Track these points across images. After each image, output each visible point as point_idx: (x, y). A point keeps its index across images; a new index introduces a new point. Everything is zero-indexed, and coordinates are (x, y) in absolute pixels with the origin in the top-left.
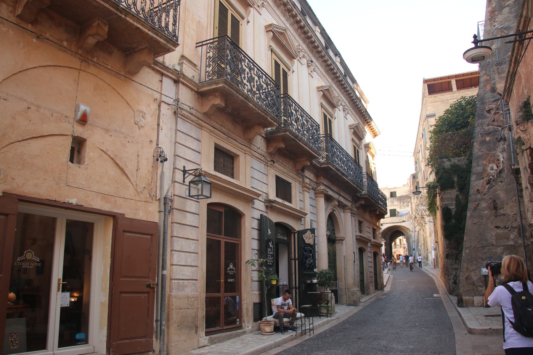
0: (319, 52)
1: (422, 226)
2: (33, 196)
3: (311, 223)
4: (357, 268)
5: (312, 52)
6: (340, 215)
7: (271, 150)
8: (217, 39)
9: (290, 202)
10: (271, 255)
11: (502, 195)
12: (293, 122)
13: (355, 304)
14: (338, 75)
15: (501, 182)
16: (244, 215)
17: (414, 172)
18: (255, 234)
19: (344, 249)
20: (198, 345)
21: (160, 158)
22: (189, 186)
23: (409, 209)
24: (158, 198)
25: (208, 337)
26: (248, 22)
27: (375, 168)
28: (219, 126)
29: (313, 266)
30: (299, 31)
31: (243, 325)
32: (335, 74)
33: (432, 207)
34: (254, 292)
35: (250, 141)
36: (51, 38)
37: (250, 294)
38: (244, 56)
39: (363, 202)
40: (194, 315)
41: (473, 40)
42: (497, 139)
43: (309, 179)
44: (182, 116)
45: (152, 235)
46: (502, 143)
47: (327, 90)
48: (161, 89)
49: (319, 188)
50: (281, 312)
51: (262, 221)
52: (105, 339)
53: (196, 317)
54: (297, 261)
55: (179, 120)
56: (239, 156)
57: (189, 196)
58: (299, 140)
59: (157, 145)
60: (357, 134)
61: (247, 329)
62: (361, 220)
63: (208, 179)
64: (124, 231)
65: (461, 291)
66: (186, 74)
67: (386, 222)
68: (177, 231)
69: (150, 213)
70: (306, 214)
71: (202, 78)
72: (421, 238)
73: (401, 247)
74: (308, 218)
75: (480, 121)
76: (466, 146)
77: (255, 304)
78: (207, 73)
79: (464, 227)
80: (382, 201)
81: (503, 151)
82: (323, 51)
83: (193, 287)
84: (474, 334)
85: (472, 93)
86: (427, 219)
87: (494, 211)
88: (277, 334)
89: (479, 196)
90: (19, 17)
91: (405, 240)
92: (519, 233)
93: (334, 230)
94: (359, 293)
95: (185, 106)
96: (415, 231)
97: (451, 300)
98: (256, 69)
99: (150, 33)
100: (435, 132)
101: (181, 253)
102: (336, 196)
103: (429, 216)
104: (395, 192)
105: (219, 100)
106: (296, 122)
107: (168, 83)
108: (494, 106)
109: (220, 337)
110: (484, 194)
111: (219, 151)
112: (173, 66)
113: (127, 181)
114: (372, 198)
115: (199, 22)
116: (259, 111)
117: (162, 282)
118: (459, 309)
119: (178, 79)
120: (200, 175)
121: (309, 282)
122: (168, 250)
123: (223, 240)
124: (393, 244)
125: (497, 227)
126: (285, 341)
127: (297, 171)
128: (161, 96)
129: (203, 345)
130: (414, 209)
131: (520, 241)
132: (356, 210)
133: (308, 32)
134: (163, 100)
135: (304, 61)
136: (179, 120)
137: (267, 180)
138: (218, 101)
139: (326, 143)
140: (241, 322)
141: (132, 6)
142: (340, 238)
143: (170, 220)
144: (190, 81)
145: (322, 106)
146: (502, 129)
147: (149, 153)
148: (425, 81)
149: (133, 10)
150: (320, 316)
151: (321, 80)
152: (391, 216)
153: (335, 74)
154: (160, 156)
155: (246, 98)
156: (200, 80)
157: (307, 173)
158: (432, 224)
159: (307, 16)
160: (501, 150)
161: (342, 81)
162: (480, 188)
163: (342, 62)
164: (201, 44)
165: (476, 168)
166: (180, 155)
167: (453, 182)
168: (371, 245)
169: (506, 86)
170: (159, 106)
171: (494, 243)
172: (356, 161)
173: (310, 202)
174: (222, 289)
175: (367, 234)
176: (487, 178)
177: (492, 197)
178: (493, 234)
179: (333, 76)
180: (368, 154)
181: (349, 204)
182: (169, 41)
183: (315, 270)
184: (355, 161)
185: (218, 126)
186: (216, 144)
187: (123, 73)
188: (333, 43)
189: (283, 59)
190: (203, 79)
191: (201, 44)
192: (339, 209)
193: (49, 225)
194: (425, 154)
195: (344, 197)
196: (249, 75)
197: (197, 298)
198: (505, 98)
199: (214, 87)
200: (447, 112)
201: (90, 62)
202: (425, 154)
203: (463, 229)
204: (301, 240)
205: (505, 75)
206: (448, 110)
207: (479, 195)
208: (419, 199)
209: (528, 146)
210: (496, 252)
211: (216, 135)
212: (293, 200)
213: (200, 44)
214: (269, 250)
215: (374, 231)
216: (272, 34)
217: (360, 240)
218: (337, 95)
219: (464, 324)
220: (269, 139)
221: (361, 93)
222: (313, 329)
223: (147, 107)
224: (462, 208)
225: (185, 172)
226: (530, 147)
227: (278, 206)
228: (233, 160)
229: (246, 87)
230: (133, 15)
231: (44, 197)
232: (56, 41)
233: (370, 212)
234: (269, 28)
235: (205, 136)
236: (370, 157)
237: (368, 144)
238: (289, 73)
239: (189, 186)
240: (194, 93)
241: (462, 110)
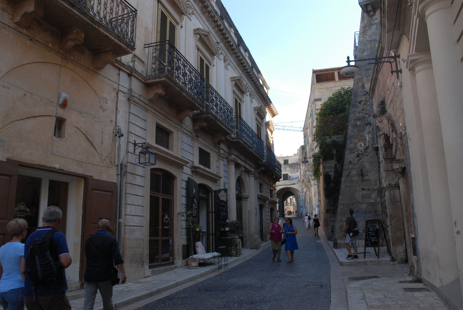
1: (308, 188)
2: (28, 162)
4: (258, 220)
5: (228, 49)
6: (246, 179)
7: (196, 128)
8: (159, 43)
9: (209, 167)
11: (367, 165)
12: (214, 107)
13: (256, 248)
15: (367, 156)
16: (176, 177)
17: (303, 144)
18: (184, 192)
21: (118, 134)
22: (139, 156)
23: (298, 174)
24: (116, 164)
25: (151, 270)
26: (182, 27)
27: (273, 141)
29: (226, 217)
30: (219, 33)
31: (175, 261)
33: (316, 173)
34: (183, 237)
35: (181, 121)
36: (40, 41)
37: (180, 239)
38: (193, 69)
39: (263, 169)
41: (347, 60)
42: (365, 123)
44: (134, 102)
45: (112, 192)
46: (368, 126)
47: (239, 80)
48: (119, 81)
49: (230, 157)
51: (189, 182)
52: (78, 270)
54: (214, 214)
55: (132, 104)
56: (173, 132)
57: (139, 163)
58: (218, 121)
59: (116, 124)
60: (260, 115)
61: (178, 265)
63: (154, 151)
64: (93, 189)
65: (336, 236)
66: (137, 69)
67: (280, 185)
68: (130, 189)
69: (110, 175)
70: (221, 178)
72: (308, 198)
73: (291, 205)
74: (222, 181)
75: (354, 109)
76: (342, 128)
77: (183, 246)
79: (340, 189)
80: (278, 168)
81: (369, 133)
82: (236, 49)
84: (344, 265)
85: (349, 84)
86: (312, 182)
87: (361, 177)
88: (201, 268)
89: (351, 166)
90: (17, 23)
91: (294, 199)
92: (378, 194)
94: (259, 240)
96: (303, 192)
97: (329, 245)
98: (182, 60)
99: (116, 40)
100: (320, 114)
101: (132, 206)
102: (243, 164)
103: (314, 180)
105: (161, 90)
106: (216, 107)
107: (123, 76)
108: (364, 99)
110: (355, 165)
111: (159, 128)
112: (128, 63)
113: (95, 151)
115: (146, 27)
117: (119, 227)
118: (335, 250)
119: (131, 73)
120: (147, 148)
121: (223, 230)
122: (123, 203)
123: (161, 196)
125: (363, 189)
126: (207, 273)
128: (119, 86)
130: (302, 174)
131: (379, 200)
132: (258, 175)
133: (226, 34)
134: (120, 89)
135: (222, 57)
136: (132, 104)
138: (160, 91)
139: (237, 122)
140: (173, 259)
141: (103, 19)
143: (124, 181)
145: (234, 93)
146: (369, 116)
147: (109, 130)
148: (314, 72)
149: (91, 13)
150: (231, 256)
151: (234, 72)
152: (284, 179)
154: (118, 132)
156: (147, 74)
157: (222, 146)
158: (316, 186)
159: (225, 20)
160: (367, 132)
161: (250, 72)
162: (351, 160)
164: (148, 46)
165: (349, 145)
166: (132, 132)
167: (333, 154)
169: (371, 87)
170: (117, 94)
171: (361, 201)
172: (259, 136)
174: (160, 234)
175: (266, 194)
176: (357, 153)
177: (360, 167)
178: (360, 194)
179: (243, 68)
180: (268, 130)
181: (253, 170)
182: (128, 45)
183: (227, 221)
184: (258, 136)
185: (158, 109)
186: (157, 123)
187: (92, 68)
188: (243, 42)
191: (148, 46)
192: (245, 174)
193: (37, 183)
194: (312, 130)
195: (249, 165)
196: (177, 65)
198: (370, 95)
199: (158, 80)
200: (330, 99)
201: (68, 59)
202: (312, 130)
203: (339, 190)
204: (217, 198)
205: (370, 78)
206: (331, 98)
207: (351, 165)
208: (307, 166)
209: (383, 133)
210: (362, 208)
212: (211, 166)
213: (147, 46)
214: (194, 205)
215: (271, 191)
216: (199, 36)
217: (261, 199)
218: (245, 83)
219: (338, 259)
220: (195, 120)
221: (264, 81)
222: (227, 265)
223: (109, 95)
224: (339, 174)
225: (135, 144)
226: (384, 133)
227: (200, 171)
228: (168, 135)
230: (104, 27)
231: (36, 163)
232: (43, 43)
234: (197, 32)
236: (269, 133)
237: (268, 122)
238: (210, 67)
239: (139, 156)
240: (142, 84)
241: (341, 98)
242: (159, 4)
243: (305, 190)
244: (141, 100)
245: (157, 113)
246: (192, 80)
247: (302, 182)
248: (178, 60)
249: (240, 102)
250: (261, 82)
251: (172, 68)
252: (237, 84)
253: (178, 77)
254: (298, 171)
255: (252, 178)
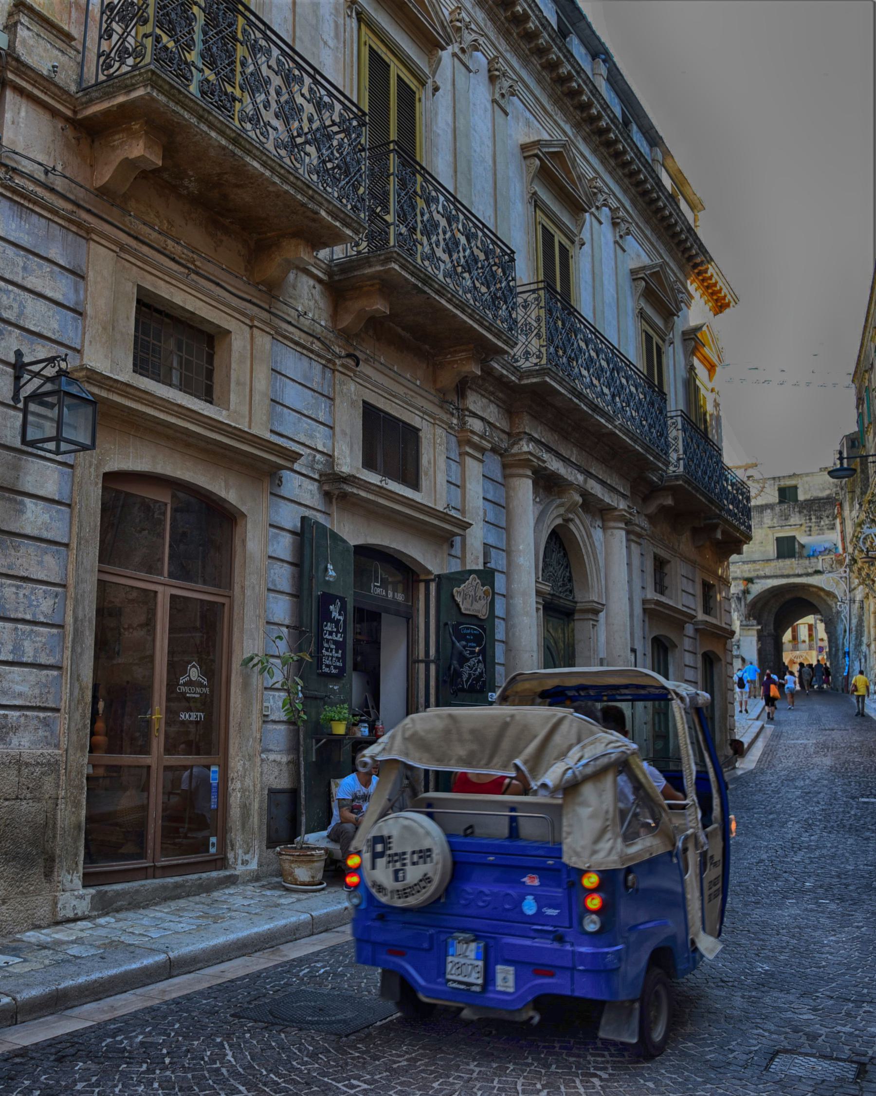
0: (541, 52)
3: (486, 555)
5: (506, 34)
6: (590, 536)
7: (346, 321)
9: (415, 485)
10: (335, 642)
14: (594, 111)
16: (244, 515)
19: (602, 638)
20: (54, 911)
25: (92, 891)
26: (436, 89)
27: (717, 405)
28: (154, 235)
31: (230, 855)
32: (584, 107)
35: (271, 291)
38: (330, 94)
39: (669, 502)
40: (40, 819)
43: (482, 419)
49: (515, 450)
50: (348, 821)
51: (308, 538)
53: (48, 825)
54: (433, 667)
56: (229, 332)
58: (437, 292)
61: (240, 869)
62: (663, 554)
67: (754, 566)
71: (85, 76)
73: (811, 648)
74: (477, 536)
78: (102, 59)
80: (734, 501)
83: (41, 733)
91: (821, 627)
93: (570, 580)
95: (25, 162)
98: (441, 198)
104: (795, 488)
109: (137, 891)
114: (697, 489)
116: (286, 187)
124: (787, 636)
127: (442, 392)
129: (71, 915)
130: (849, 537)
132: (645, 524)
135: (480, 60)
137: (332, 413)
138: (137, 149)
140: (223, 846)
142: (589, 606)
144: (46, 82)
145: (536, 202)
151: (532, 123)
153: (584, 107)
155: (235, 141)
157: (475, 402)
163: (615, 79)
168: (696, 630)
173: (484, 491)
174: (158, 743)
175: (684, 597)
179: (578, 115)
180: (696, 362)
181: (622, 505)
189: (399, 47)
190: (90, 76)
192: (587, 520)
196: (468, 252)
197: (52, 766)
199: (121, 99)
204: (448, 603)
208: (866, 506)
211: (145, 262)
212: (424, 483)
215: (708, 590)
217: (653, 613)
218: (591, 174)
220: (339, 286)
221: (679, 179)
227: (363, 494)
229: (442, 266)
233: (696, 532)
235: (101, 262)
236: (701, 371)
242: (363, 26)
243: (859, 595)
244: (52, 190)
245: (145, 249)
246: (476, 260)
247: (850, 566)
248: (254, 49)
249: (660, 342)
250: (667, 182)
251: (413, 230)
252: (549, 169)
253: (431, 257)
254: (832, 527)
255: (619, 536)
